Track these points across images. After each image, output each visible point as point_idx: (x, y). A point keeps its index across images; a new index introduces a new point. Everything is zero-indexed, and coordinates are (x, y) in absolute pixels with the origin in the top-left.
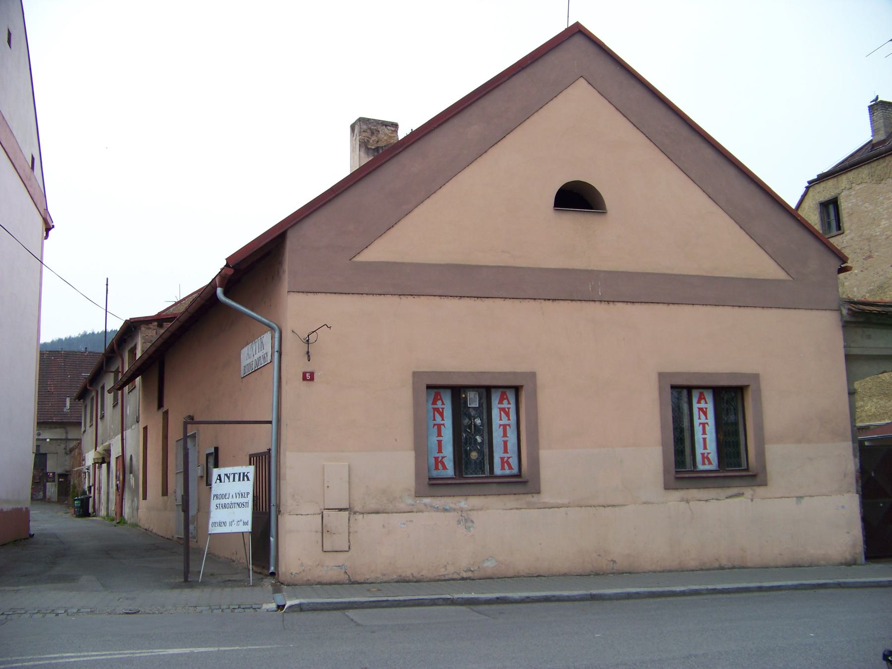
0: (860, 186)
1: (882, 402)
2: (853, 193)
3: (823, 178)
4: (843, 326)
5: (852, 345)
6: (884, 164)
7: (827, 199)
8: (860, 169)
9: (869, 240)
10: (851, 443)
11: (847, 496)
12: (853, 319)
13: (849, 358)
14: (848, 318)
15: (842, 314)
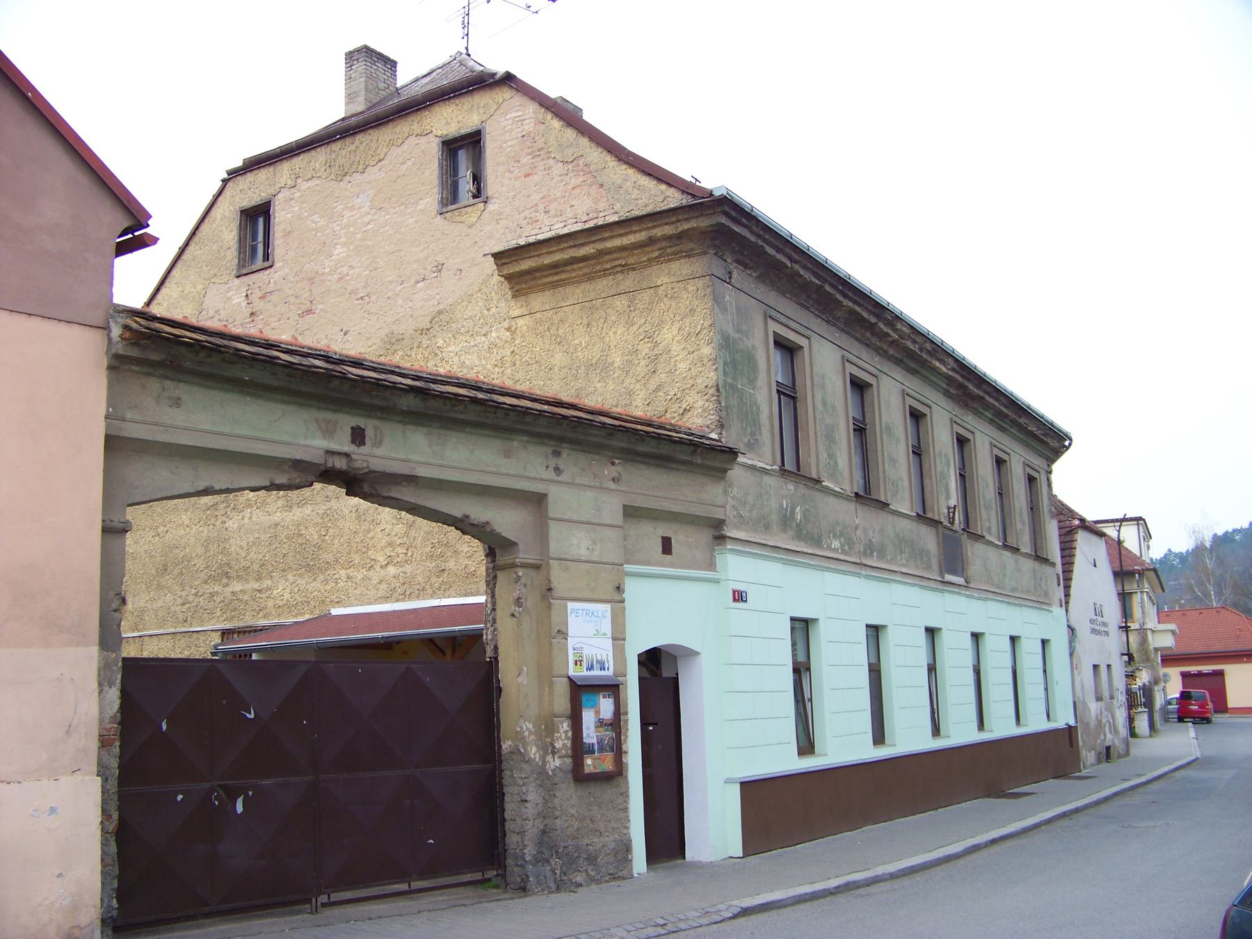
0: (310, 184)
1: (301, 582)
2: (297, 194)
3: (255, 164)
4: (110, 368)
5: (128, 415)
6: (353, 147)
7: (253, 203)
8: (313, 153)
9: (311, 280)
10: (94, 650)
11: (67, 781)
12: (134, 352)
13: (114, 445)
14: (120, 349)
15: (110, 339)
